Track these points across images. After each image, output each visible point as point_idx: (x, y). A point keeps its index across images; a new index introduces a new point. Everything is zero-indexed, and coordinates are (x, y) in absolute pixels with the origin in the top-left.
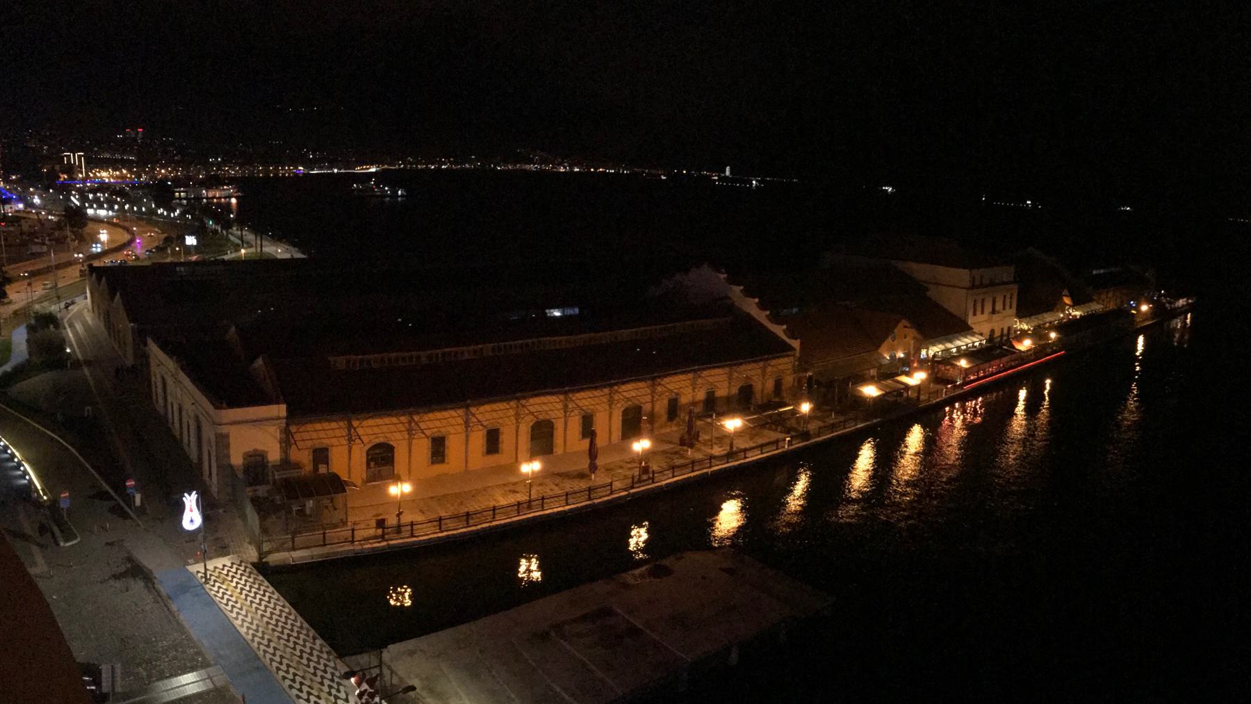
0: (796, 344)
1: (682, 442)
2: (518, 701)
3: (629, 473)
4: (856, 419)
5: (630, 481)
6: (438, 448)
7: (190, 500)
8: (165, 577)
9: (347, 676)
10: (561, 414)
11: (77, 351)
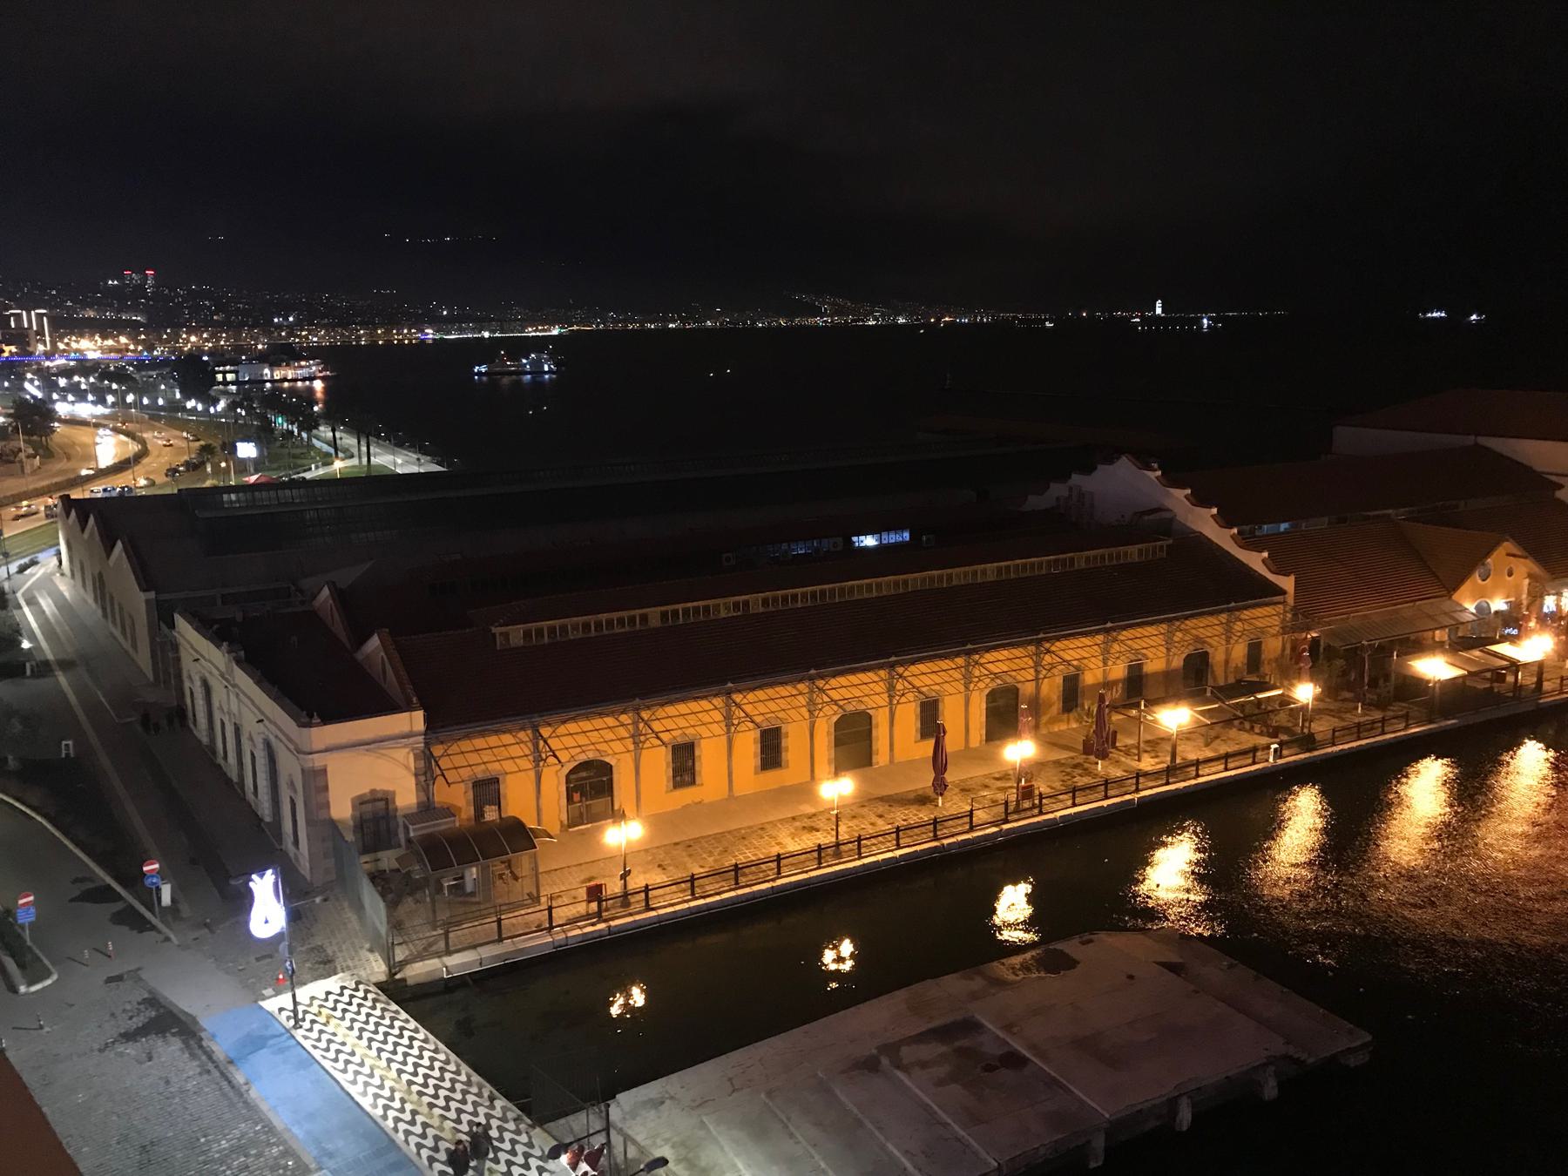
0: (1288, 583)
1: (1087, 749)
2: (831, 1173)
3: (1001, 797)
5: (1001, 809)
7: (264, 886)
8: (221, 1027)
9: (554, 1154)
10: (882, 700)
11: (44, 644)
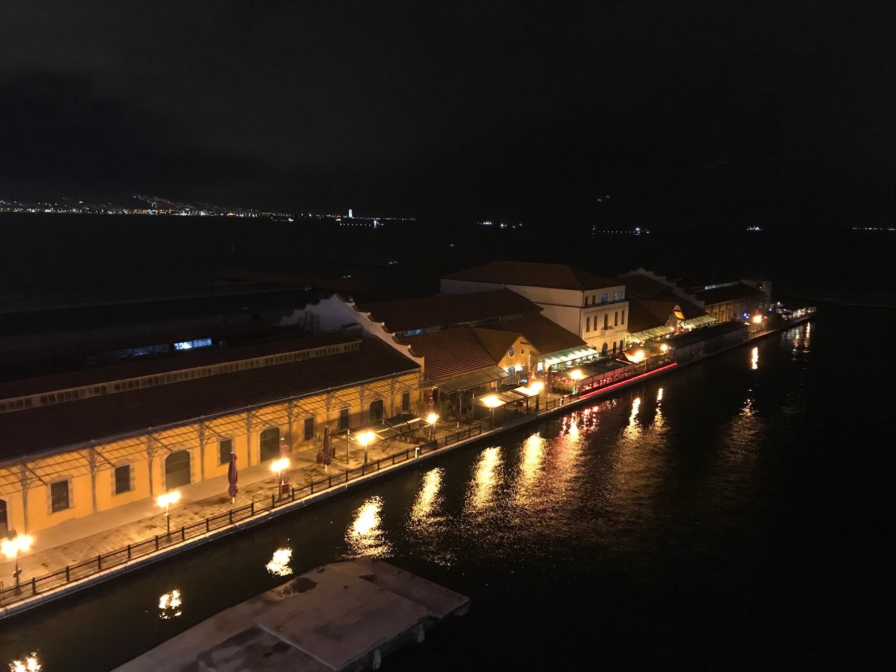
0: (421, 361)
3: (270, 493)
4: (480, 429)
5: (270, 500)
6: (60, 495)
10: (196, 443)
